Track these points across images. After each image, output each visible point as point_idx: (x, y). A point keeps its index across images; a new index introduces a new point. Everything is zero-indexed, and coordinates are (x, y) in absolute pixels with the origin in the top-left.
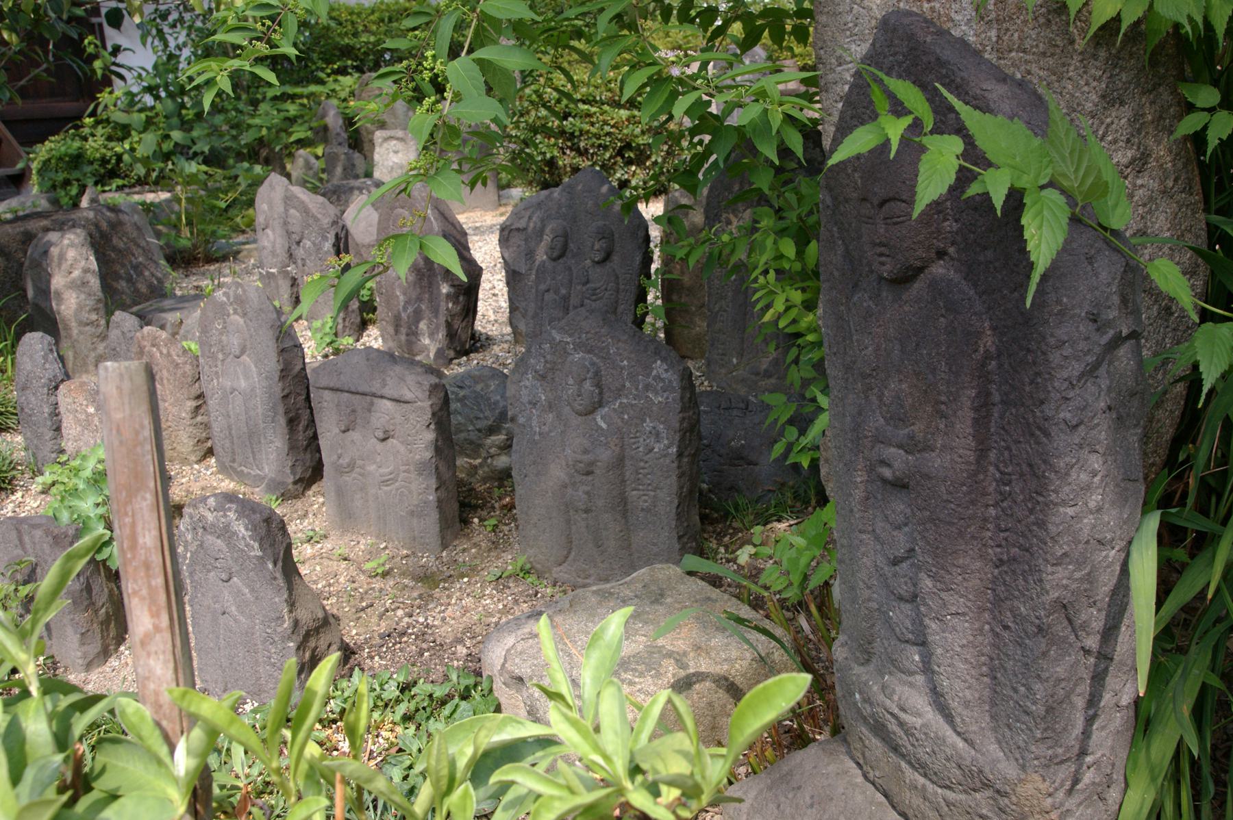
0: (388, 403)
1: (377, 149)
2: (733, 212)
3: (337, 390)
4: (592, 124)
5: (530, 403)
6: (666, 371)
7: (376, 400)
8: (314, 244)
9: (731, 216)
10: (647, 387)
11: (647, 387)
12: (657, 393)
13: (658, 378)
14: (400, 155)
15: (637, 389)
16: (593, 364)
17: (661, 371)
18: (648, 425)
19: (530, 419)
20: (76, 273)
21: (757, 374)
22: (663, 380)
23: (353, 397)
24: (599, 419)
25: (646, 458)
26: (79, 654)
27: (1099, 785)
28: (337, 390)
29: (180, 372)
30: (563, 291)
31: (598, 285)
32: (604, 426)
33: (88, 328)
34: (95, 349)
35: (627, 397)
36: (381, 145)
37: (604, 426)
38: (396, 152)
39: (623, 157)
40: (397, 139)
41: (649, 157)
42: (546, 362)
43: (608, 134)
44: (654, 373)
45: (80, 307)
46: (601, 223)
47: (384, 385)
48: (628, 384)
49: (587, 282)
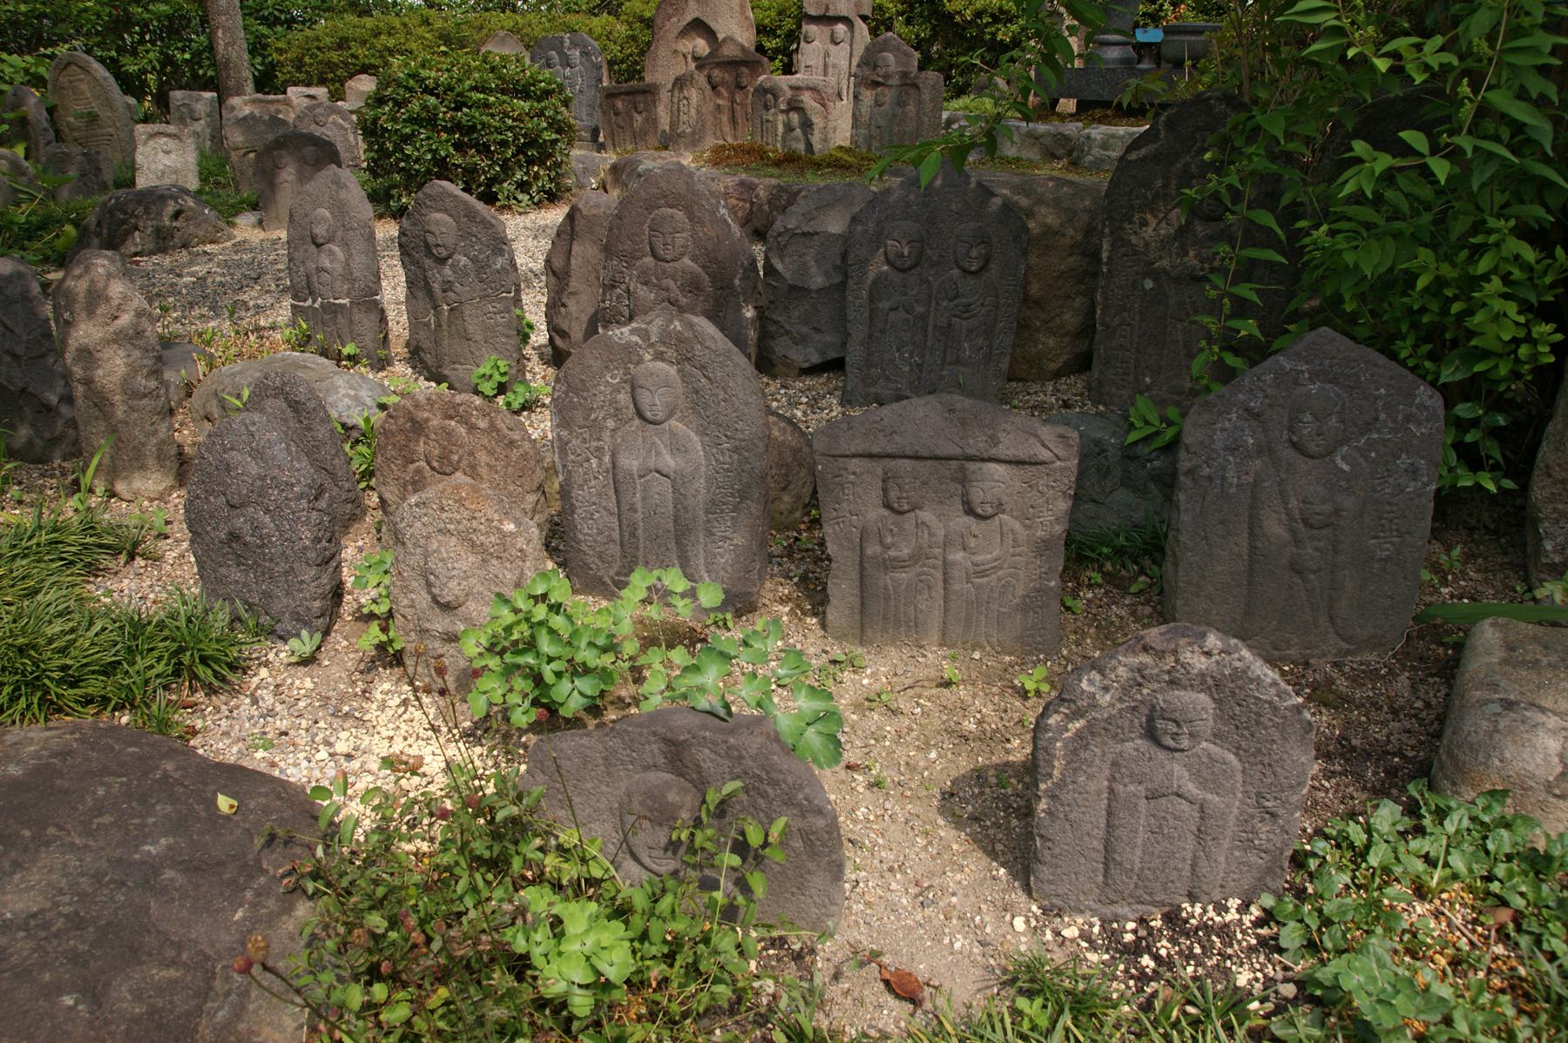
0: (999, 469)
1: (140, 149)
2: (1151, 212)
3: (1023, 463)
4: (492, 115)
5: (1226, 448)
6: (1431, 397)
7: (971, 466)
8: (474, 260)
9: (1149, 217)
10: (1409, 418)
11: (1409, 418)
12: (1419, 424)
13: (1422, 406)
14: (173, 156)
15: (1395, 421)
16: (1338, 395)
17: (1425, 397)
18: (1404, 461)
19: (1224, 469)
20: (125, 319)
21: (1182, 393)
22: (1426, 408)
23: (919, 464)
24: (1339, 461)
25: (1395, 500)
26: (1373, 940)
27: (507, 719)
28: (1023, 463)
29: (515, 454)
30: (920, 309)
31: (972, 300)
32: (1346, 467)
33: (145, 401)
34: (155, 432)
35: (1379, 432)
36: (145, 143)
37: (1346, 467)
38: (168, 153)
39: (525, 154)
40: (169, 135)
41: (551, 155)
42: (1266, 396)
43: (510, 128)
44: (1418, 401)
45: (134, 370)
46: (972, 225)
47: (994, 441)
48: (1382, 416)
49: (955, 297)
